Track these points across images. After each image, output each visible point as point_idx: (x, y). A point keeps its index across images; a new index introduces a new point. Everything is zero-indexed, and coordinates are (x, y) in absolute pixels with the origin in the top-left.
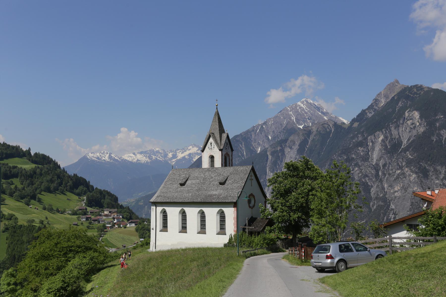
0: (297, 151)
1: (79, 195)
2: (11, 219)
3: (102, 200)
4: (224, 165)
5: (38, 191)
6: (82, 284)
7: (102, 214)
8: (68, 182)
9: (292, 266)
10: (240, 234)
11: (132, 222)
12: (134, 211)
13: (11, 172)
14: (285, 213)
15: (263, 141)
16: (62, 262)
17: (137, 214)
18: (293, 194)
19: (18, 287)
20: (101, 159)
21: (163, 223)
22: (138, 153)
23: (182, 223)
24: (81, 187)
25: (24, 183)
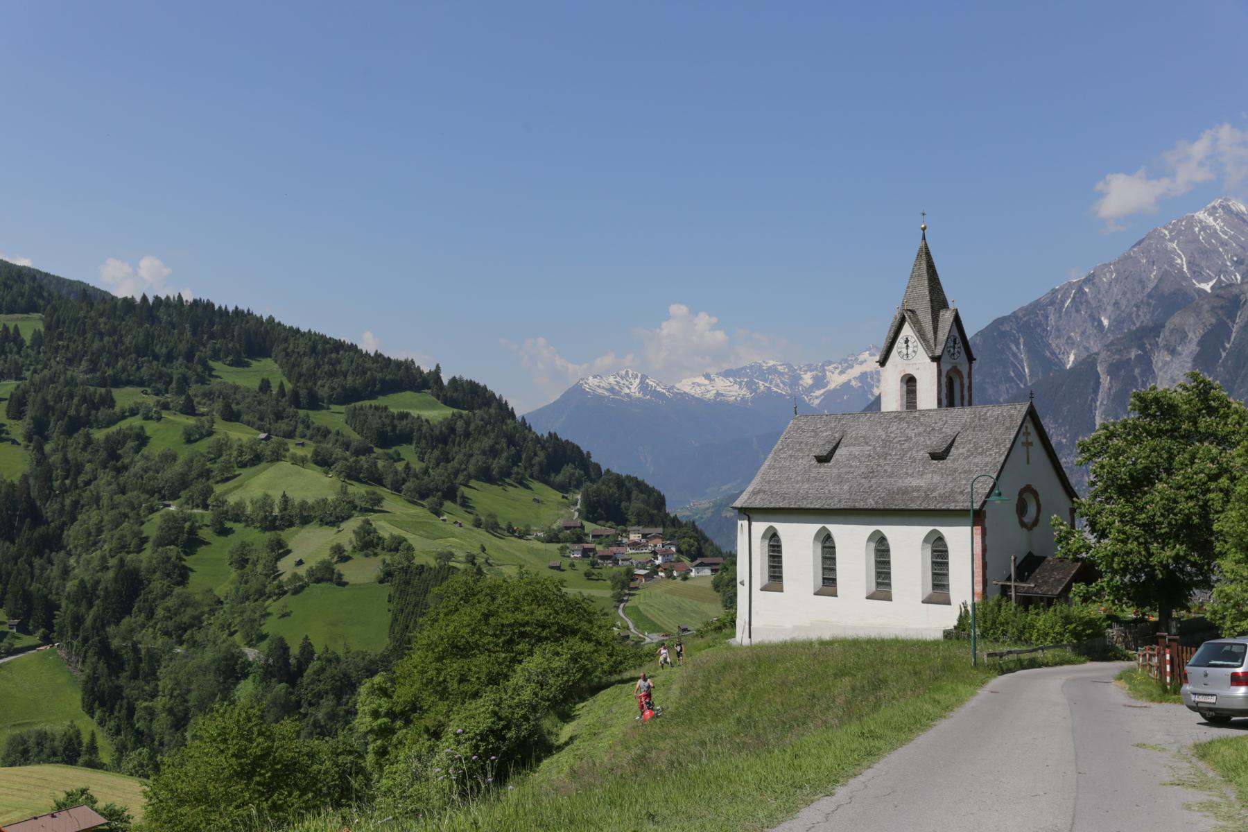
0: (1195, 360)
1: (563, 488)
2: (397, 550)
3: (624, 504)
4: (944, 401)
5: (461, 478)
6: (547, 724)
7: (625, 540)
8: (535, 455)
9: (1133, 702)
10: (991, 603)
11: (702, 565)
12: (708, 534)
13: (394, 427)
14: (1132, 545)
15: (1083, 333)
16: (500, 664)
17: (717, 542)
18: (1159, 486)
19: (399, 723)
20: (618, 393)
21: (770, 567)
22: (719, 374)
23: (824, 569)
24: (568, 469)
25: (427, 456)
